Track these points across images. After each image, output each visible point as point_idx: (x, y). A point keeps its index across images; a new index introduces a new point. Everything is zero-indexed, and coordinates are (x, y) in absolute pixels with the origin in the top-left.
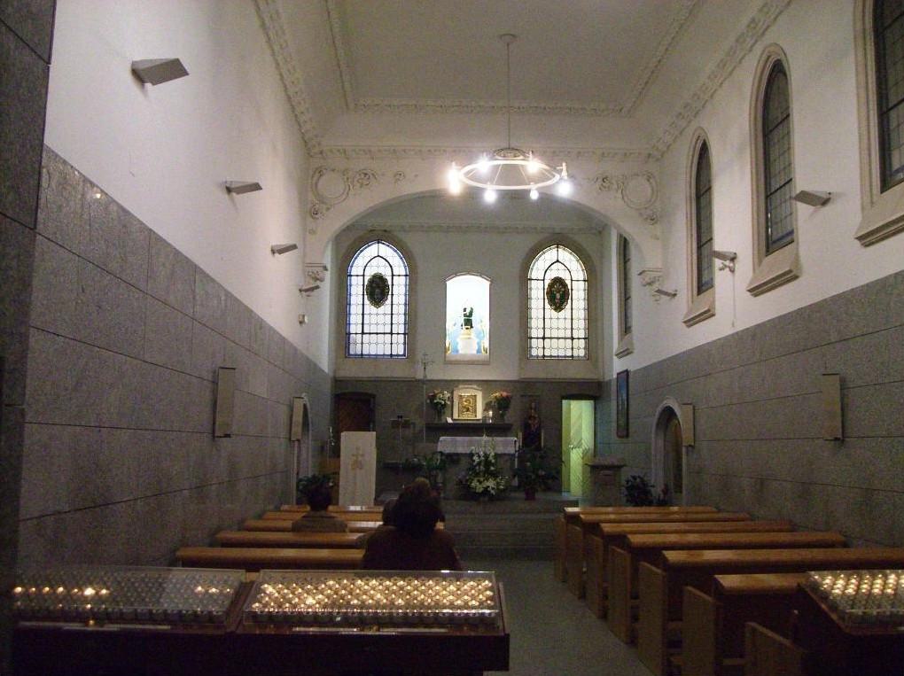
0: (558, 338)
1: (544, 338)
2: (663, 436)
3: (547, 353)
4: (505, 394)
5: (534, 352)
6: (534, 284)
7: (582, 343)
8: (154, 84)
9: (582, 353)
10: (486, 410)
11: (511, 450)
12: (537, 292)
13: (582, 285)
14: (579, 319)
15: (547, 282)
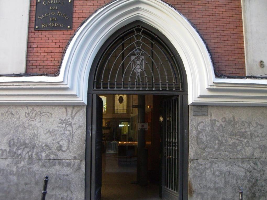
0: (121, 109)
1: (118, 109)
2: (32, 46)
3: (118, 112)
4: (109, 121)
5: (116, 112)
6: (116, 98)
7: (126, 110)
8: (102, 99)
9: (126, 112)
10: (105, 124)
11: (108, 132)
12: (117, 99)
13: (126, 98)
14: (117, 101)
15: (119, 97)
